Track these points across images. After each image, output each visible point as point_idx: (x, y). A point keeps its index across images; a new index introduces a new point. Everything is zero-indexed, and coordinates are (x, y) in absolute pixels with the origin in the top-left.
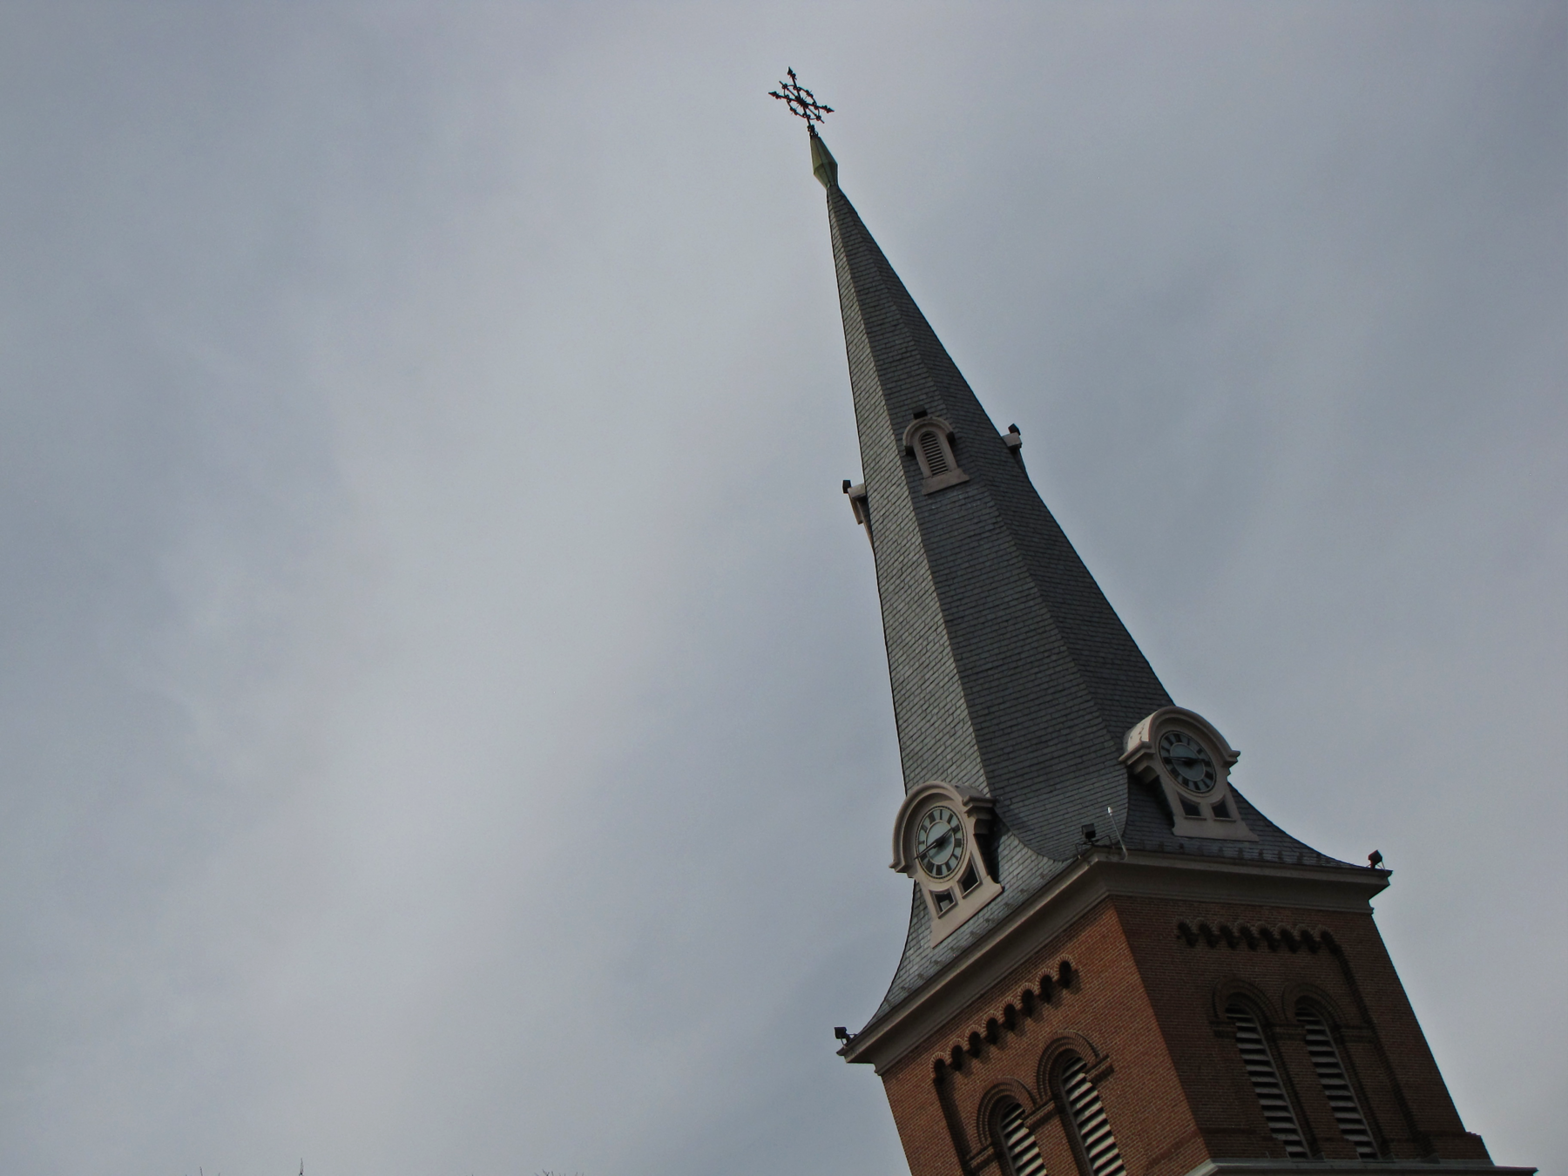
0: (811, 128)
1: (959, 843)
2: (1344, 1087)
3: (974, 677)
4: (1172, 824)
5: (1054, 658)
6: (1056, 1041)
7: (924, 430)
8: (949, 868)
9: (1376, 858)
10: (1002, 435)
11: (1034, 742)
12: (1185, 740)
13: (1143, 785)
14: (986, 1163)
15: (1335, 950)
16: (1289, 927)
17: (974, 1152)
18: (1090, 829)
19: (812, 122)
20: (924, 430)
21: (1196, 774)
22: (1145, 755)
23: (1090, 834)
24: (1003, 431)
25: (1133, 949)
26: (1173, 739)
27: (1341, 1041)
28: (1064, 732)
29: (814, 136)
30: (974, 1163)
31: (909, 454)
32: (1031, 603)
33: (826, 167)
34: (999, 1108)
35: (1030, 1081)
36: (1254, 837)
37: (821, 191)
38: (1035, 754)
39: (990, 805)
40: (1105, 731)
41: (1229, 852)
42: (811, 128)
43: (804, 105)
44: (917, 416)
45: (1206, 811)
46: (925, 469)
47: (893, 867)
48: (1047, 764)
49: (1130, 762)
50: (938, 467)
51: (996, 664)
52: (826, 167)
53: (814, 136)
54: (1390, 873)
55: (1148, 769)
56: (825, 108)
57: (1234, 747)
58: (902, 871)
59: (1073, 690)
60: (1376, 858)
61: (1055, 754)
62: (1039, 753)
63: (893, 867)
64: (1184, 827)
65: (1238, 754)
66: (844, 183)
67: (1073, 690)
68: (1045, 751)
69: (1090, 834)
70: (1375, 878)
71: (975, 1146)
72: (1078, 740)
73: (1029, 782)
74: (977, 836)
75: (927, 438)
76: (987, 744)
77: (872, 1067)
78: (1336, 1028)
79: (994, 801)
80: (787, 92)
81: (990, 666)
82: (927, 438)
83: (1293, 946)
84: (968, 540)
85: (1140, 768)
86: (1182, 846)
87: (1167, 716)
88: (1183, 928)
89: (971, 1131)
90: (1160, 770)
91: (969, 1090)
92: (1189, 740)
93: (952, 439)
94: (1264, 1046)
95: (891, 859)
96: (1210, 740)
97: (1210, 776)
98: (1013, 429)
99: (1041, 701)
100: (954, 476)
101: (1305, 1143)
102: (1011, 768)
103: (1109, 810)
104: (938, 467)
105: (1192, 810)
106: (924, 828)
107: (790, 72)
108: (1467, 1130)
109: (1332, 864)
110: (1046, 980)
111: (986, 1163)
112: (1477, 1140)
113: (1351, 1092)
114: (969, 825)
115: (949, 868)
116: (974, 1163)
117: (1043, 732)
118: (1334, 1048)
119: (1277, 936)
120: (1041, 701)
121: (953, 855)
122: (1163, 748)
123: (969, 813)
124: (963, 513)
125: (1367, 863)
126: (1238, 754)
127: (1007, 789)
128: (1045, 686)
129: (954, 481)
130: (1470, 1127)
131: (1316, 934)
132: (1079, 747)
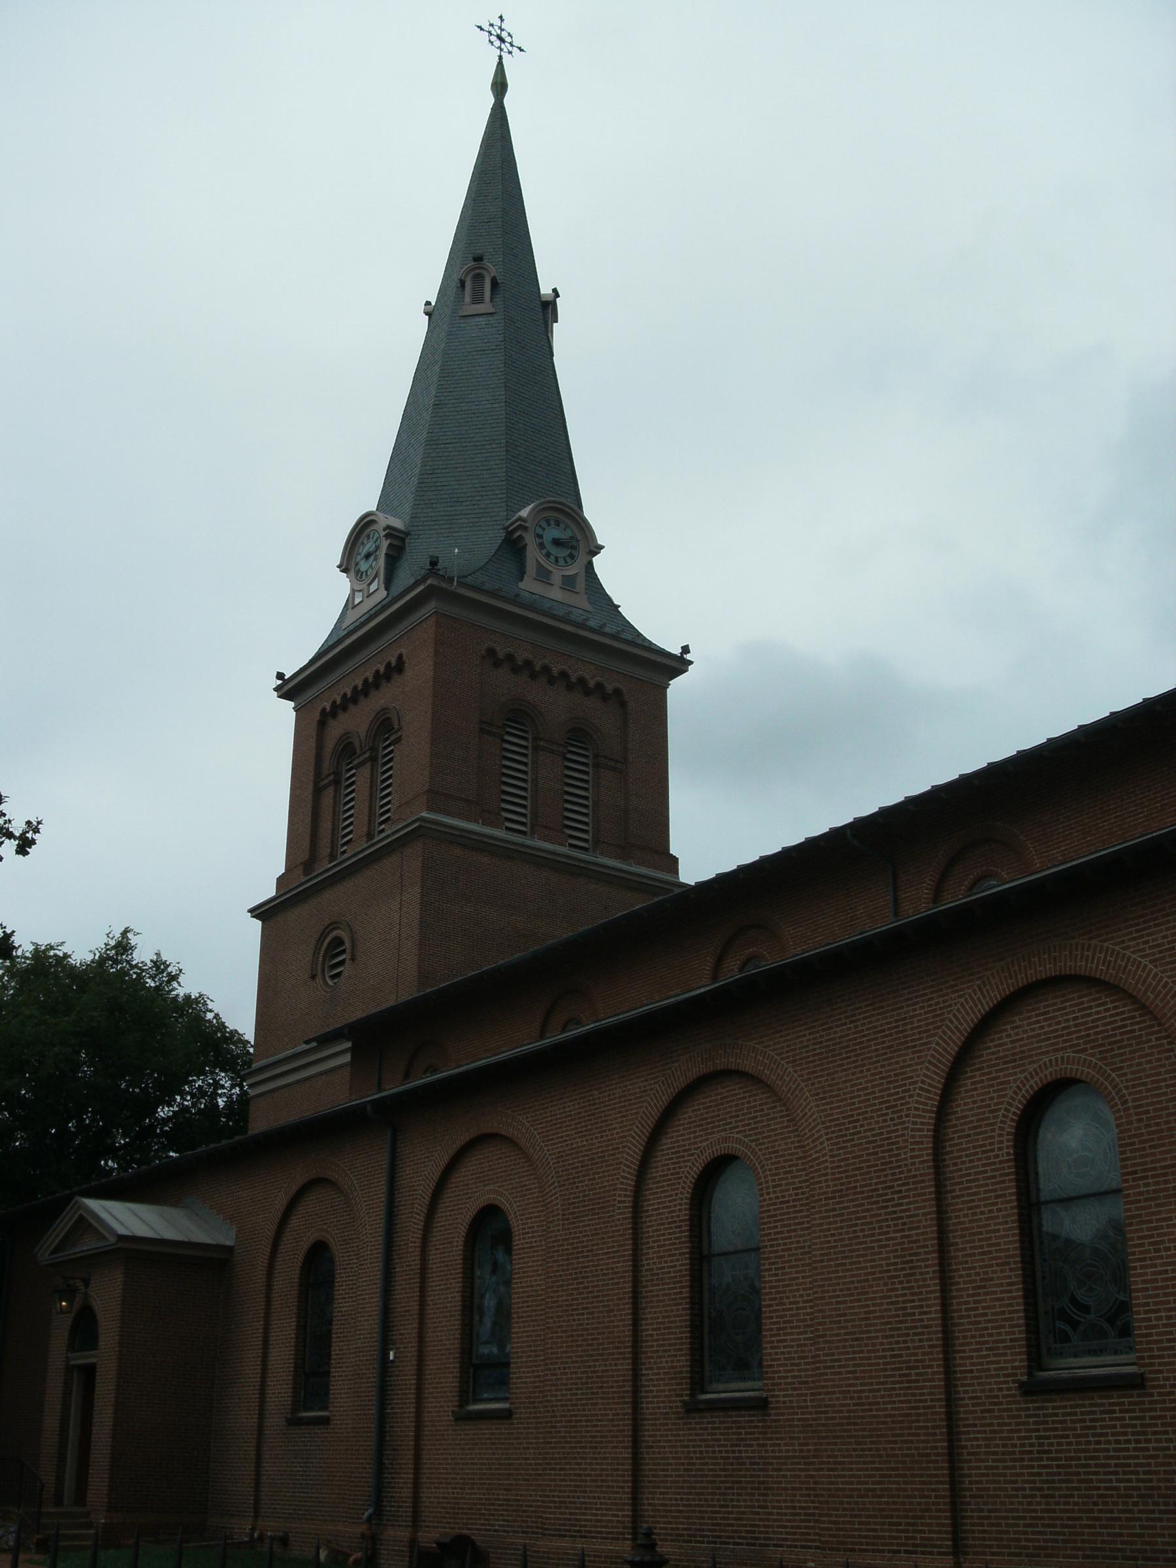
0: (500, 57)
1: (376, 559)
2: (586, 798)
4: (522, 580)
5: (494, 446)
6: (384, 710)
7: (477, 271)
8: (367, 575)
9: (686, 649)
10: (542, 292)
12: (562, 526)
13: (513, 546)
14: (329, 785)
15: (623, 704)
18: (435, 560)
20: (477, 271)
23: (434, 563)
24: (545, 289)
25: (436, 653)
27: (597, 766)
29: (500, 63)
30: (323, 783)
31: (462, 284)
32: (496, 405)
33: (500, 86)
34: (346, 749)
36: (589, 607)
37: (490, 100)
40: (504, 504)
41: (560, 612)
42: (500, 57)
43: (502, 40)
45: (557, 576)
46: (468, 299)
47: (338, 567)
48: (456, 517)
50: (477, 299)
52: (500, 86)
53: (500, 63)
54: (691, 663)
55: (520, 537)
56: (482, 29)
57: (600, 542)
59: (496, 471)
60: (686, 649)
61: (464, 512)
63: (338, 567)
64: (529, 585)
65: (602, 547)
66: (507, 101)
67: (496, 471)
69: (434, 563)
70: (677, 664)
75: (478, 278)
77: (292, 704)
78: (596, 756)
79: (407, 534)
80: (491, 29)
81: (448, 441)
82: (478, 278)
83: (587, 692)
84: (475, 353)
87: (546, 505)
88: (491, 652)
90: (530, 539)
91: (336, 729)
92: (567, 527)
93: (495, 284)
96: (586, 537)
97: (572, 556)
98: (556, 293)
99: (471, 473)
103: (456, 550)
104: (477, 299)
105: (544, 575)
106: (363, 543)
107: (501, 17)
109: (646, 644)
110: (389, 664)
111: (329, 785)
114: (385, 544)
115: (367, 575)
116: (323, 783)
118: (590, 770)
119: (573, 679)
120: (471, 473)
121: (371, 566)
122: (540, 526)
125: (677, 651)
126: (602, 547)
129: (483, 311)
130: (673, 851)
131: (609, 688)
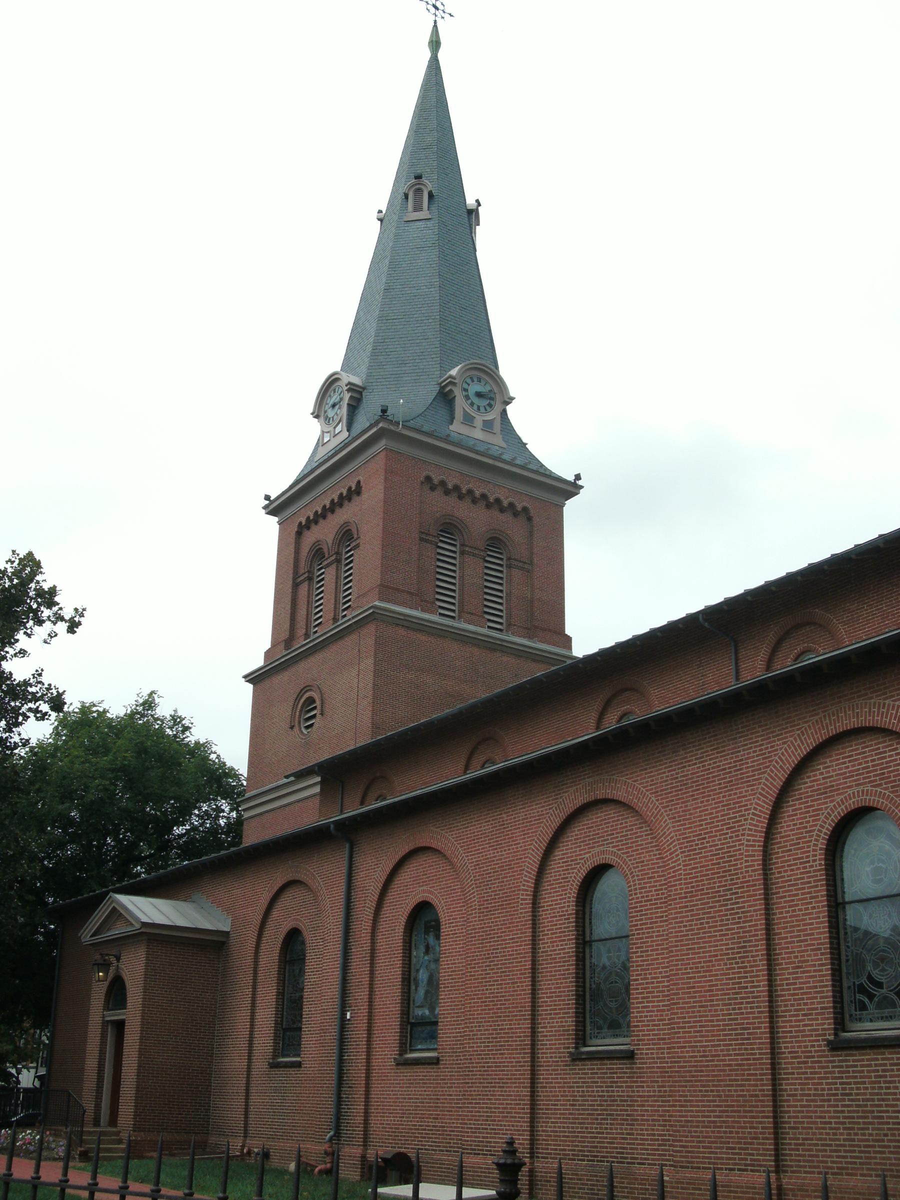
0: (435, 22)
1: (340, 408)
3: (385, 321)
4: (451, 423)
6: (347, 523)
7: (417, 187)
9: (578, 477)
11: (400, 362)
13: (445, 397)
14: (303, 581)
15: (530, 519)
16: (502, 498)
17: (301, 573)
19: (437, 19)
20: (417, 187)
21: (484, 403)
22: (450, 382)
23: (384, 411)
24: (470, 201)
26: (475, 380)
28: (417, 361)
29: (435, 26)
33: (435, 44)
35: (330, 542)
36: (504, 445)
37: (428, 55)
38: (397, 369)
39: (361, 390)
42: (435, 22)
44: (416, 178)
47: (312, 414)
49: (443, 385)
50: (418, 208)
51: (399, 317)
52: (435, 44)
53: (435, 26)
57: (512, 394)
58: (315, 417)
60: (578, 477)
62: (399, 369)
63: (312, 414)
65: (513, 399)
66: (440, 55)
68: (403, 369)
69: (384, 411)
71: (302, 571)
72: (422, 367)
73: (387, 383)
74: (348, 404)
75: (419, 192)
76: (374, 357)
77: (276, 519)
85: (448, 389)
86: (448, 436)
88: (428, 479)
89: (302, 563)
91: (309, 538)
93: (431, 196)
94: (457, 556)
95: (311, 411)
97: (490, 405)
99: (412, 342)
100: (424, 214)
101: (457, 612)
102: (382, 374)
103: (402, 401)
104: (418, 208)
108: (566, 633)
111: (303, 581)
112: (569, 639)
113: (504, 595)
114: (347, 396)
117: (406, 359)
118: (504, 569)
122: (466, 382)
123: (348, 390)
124: (419, 235)
125: (571, 478)
126: (513, 399)
127: (374, 384)
128: (419, 335)
131: (519, 507)
132: (421, 371)
